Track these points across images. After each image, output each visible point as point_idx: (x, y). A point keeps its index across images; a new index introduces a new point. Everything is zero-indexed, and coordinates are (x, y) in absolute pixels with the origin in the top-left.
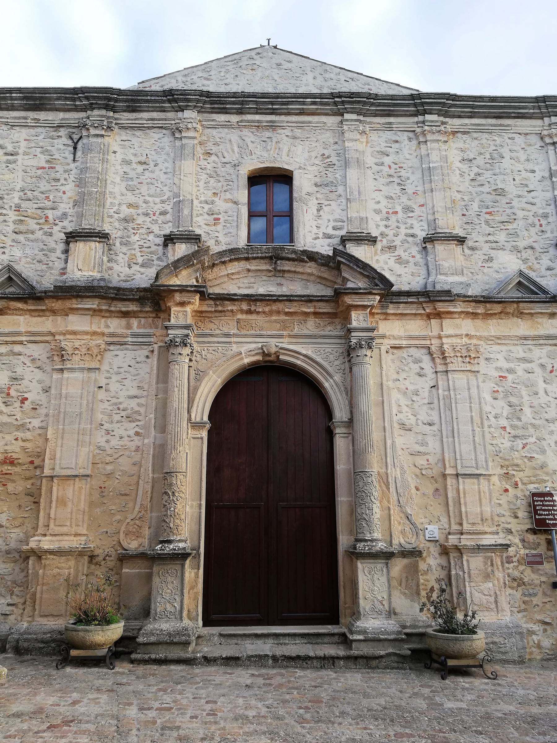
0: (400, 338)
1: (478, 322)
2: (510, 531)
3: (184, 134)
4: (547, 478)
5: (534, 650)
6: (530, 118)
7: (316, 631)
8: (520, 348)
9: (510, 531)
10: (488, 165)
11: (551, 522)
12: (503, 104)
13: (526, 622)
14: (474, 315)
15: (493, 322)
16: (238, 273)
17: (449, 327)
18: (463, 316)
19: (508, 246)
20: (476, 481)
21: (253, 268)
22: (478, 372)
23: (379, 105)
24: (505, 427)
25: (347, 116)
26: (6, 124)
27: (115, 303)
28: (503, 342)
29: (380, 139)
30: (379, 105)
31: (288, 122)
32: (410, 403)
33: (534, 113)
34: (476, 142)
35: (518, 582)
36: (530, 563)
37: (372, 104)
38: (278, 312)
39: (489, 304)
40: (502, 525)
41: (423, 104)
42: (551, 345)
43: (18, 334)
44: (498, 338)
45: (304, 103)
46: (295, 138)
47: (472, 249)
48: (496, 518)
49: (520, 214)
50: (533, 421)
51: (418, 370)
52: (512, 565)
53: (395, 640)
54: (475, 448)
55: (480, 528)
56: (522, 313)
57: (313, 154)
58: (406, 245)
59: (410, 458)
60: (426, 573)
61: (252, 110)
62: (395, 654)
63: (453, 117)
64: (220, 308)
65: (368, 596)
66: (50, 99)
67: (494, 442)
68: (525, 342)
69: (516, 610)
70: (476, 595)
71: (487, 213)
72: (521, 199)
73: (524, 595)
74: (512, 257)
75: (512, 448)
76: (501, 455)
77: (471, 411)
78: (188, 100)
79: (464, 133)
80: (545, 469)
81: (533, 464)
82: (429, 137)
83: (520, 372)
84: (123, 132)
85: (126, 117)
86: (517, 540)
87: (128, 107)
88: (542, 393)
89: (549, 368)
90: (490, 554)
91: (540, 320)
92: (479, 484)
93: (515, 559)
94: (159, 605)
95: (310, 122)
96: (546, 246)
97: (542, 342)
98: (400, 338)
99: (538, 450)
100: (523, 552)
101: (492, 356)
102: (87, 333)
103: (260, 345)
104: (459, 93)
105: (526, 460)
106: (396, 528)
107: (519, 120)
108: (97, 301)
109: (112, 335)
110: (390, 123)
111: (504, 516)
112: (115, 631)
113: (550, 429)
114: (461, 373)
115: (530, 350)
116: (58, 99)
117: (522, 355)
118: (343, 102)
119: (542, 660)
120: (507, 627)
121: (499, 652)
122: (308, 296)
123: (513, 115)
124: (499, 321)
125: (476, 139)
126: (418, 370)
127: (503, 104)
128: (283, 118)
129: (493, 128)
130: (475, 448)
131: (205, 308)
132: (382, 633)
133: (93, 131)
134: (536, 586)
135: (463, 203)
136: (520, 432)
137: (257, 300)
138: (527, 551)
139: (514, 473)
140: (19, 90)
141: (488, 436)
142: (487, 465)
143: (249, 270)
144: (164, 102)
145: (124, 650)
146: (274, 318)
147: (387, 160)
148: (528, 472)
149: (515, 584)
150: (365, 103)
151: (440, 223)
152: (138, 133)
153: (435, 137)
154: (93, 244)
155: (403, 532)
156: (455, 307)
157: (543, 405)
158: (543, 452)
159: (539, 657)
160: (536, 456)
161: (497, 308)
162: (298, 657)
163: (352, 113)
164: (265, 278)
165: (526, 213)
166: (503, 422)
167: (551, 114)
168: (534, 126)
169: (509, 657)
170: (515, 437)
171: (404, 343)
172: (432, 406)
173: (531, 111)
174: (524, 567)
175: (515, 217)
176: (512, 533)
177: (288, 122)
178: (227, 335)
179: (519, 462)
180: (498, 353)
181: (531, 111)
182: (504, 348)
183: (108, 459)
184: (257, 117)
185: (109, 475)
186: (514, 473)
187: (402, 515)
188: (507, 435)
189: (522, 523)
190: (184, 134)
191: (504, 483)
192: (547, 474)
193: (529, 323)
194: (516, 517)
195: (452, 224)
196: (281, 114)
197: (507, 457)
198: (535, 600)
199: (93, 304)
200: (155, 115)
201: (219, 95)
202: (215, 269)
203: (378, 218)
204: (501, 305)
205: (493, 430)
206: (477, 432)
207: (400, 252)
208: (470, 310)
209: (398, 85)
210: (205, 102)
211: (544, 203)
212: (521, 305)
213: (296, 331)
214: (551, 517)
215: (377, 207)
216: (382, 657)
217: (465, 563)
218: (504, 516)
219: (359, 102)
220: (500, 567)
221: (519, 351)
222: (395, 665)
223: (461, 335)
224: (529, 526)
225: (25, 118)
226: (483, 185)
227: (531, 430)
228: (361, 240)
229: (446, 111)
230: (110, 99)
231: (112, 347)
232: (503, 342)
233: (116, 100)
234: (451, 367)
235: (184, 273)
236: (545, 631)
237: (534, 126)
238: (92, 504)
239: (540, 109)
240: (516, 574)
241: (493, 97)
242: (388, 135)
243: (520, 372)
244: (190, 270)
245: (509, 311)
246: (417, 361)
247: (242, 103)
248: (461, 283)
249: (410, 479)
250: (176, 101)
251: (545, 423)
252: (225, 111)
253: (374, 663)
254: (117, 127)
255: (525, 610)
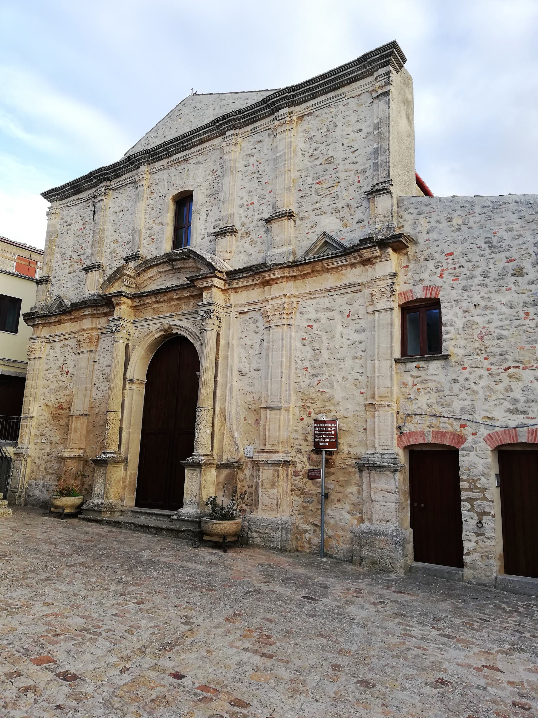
0: (242, 305)
1: (299, 282)
2: (300, 451)
3: (139, 184)
4: (331, 408)
5: (306, 544)
6: (362, 78)
7: (150, 511)
8: (326, 300)
9: (300, 451)
10: (324, 138)
11: (321, 444)
12: (332, 77)
13: (303, 523)
14: (295, 278)
15: (309, 280)
16: (155, 275)
17: (275, 290)
18: (285, 280)
19: (329, 209)
20: (278, 412)
21: (161, 270)
22: (291, 324)
23: (245, 116)
24: (306, 368)
25: (228, 133)
26: (68, 206)
27: (98, 308)
28: (314, 296)
29: (248, 145)
30: (245, 116)
31: (193, 153)
32: (247, 355)
33: (362, 73)
34: (317, 119)
35: (302, 492)
36: (310, 477)
37: (241, 118)
38: (173, 299)
39: (302, 267)
40: (296, 447)
41: (273, 103)
42: (350, 293)
43: (64, 334)
44: (310, 294)
45: (199, 135)
46: (198, 163)
47: (302, 219)
48: (292, 441)
49: (343, 176)
50: (328, 361)
51: (255, 329)
52: (298, 477)
53: (192, 521)
54: (281, 386)
55: (275, 448)
56: (327, 268)
57: (207, 173)
58: (257, 228)
59: (243, 396)
60: (242, 481)
61: (174, 152)
62: (191, 531)
63: (300, 103)
64: (142, 303)
65: (189, 492)
66: (81, 185)
67: (297, 381)
68: (330, 294)
69: (297, 512)
70: (265, 497)
71: (317, 183)
72: (345, 161)
73: (304, 501)
74: (332, 218)
75: (309, 385)
76: (302, 391)
77: (282, 357)
78: (139, 160)
79: (309, 114)
80: (331, 401)
81: (323, 397)
82: (279, 130)
83: (324, 320)
84: (114, 193)
85: (114, 183)
86: (305, 459)
87: (114, 175)
88: (338, 336)
89: (346, 314)
90: (277, 468)
91: (344, 272)
92: (280, 415)
93: (301, 473)
94: (98, 489)
95: (206, 148)
96: (360, 201)
97: (342, 291)
98: (242, 305)
99: (329, 385)
100: (308, 468)
101: (305, 310)
102: (89, 329)
103: (159, 325)
104: (296, 83)
105: (319, 394)
106: (226, 447)
107: (354, 84)
108: (90, 309)
109: (101, 328)
110: (255, 128)
111: (298, 439)
112: (74, 500)
113: (340, 367)
114: (279, 327)
115: (334, 299)
116: (84, 183)
117: (327, 305)
118: (221, 125)
119: (310, 553)
120: (277, 523)
121: (269, 541)
122: (182, 285)
123: (346, 82)
124: (315, 278)
125: (317, 116)
126: (255, 329)
127: (332, 77)
128: (193, 150)
129: (331, 101)
130: (281, 386)
131: (136, 304)
132: (188, 516)
133: (99, 198)
134: (313, 495)
135: (301, 180)
136: (317, 371)
137: (157, 294)
138: (311, 468)
139: (309, 405)
140: (68, 185)
141: (293, 376)
142: (289, 399)
143: (160, 272)
144: (129, 166)
145: (78, 513)
146: (172, 303)
147: (252, 160)
148: (319, 404)
149: (299, 493)
150: (235, 120)
151: (279, 204)
152: (121, 191)
153: (283, 129)
154: (94, 273)
155: (230, 451)
156: (275, 274)
157: (337, 347)
158: (332, 386)
159: (308, 551)
160: (326, 390)
161: (308, 269)
162: (144, 526)
163: (230, 130)
164: (171, 275)
165: (348, 173)
166: (307, 364)
167: (377, 67)
168: (364, 85)
169: (274, 545)
170: (313, 375)
171: (246, 309)
172: (260, 355)
173: (360, 72)
174: (306, 480)
175: (339, 180)
176: (301, 452)
177: (193, 153)
178: (146, 320)
179: (313, 395)
180: (310, 307)
181: (360, 72)
182: (314, 301)
183: (97, 405)
184: (179, 155)
185: (97, 414)
186: (309, 405)
187: (231, 438)
188: (308, 374)
189: (307, 447)
190: (139, 184)
191: (302, 413)
192: (333, 405)
193: (336, 276)
194: (307, 441)
195: (288, 202)
196: (191, 148)
197: (306, 392)
198: (310, 507)
199: (88, 311)
200: (128, 175)
201: (153, 150)
202: (141, 276)
203: (241, 211)
204: (309, 266)
205: (298, 371)
206: (284, 374)
207: (253, 236)
208: (287, 275)
209: (267, 90)
210: (148, 157)
211: (365, 158)
212: (324, 262)
213: (184, 311)
214: (322, 440)
215: (241, 202)
216: (183, 531)
217: (261, 474)
218: (298, 439)
219: (230, 120)
220: (285, 479)
221: (325, 302)
222: (191, 537)
223: (280, 296)
224: (313, 448)
225: (74, 200)
226: (318, 158)
227: (325, 368)
228: (225, 233)
229: (294, 101)
230: (105, 174)
231: (102, 336)
232: (314, 296)
233: (108, 174)
234: (272, 323)
235: (116, 284)
236: (315, 531)
237: (364, 85)
238: (88, 431)
239: (365, 67)
240: (300, 485)
241: (323, 75)
242: (256, 138)
243: (324, 320)
244: (119, 281)
245: (317, 269)
246: (256, 321)
247: (167, 150)
248: (284, 253)
249: (241, 412)
250: (133, 163)
251: (337, 361)
252: (160, 159)
253: (181, 535)
254: (111, 192)
255: (303, 513)
